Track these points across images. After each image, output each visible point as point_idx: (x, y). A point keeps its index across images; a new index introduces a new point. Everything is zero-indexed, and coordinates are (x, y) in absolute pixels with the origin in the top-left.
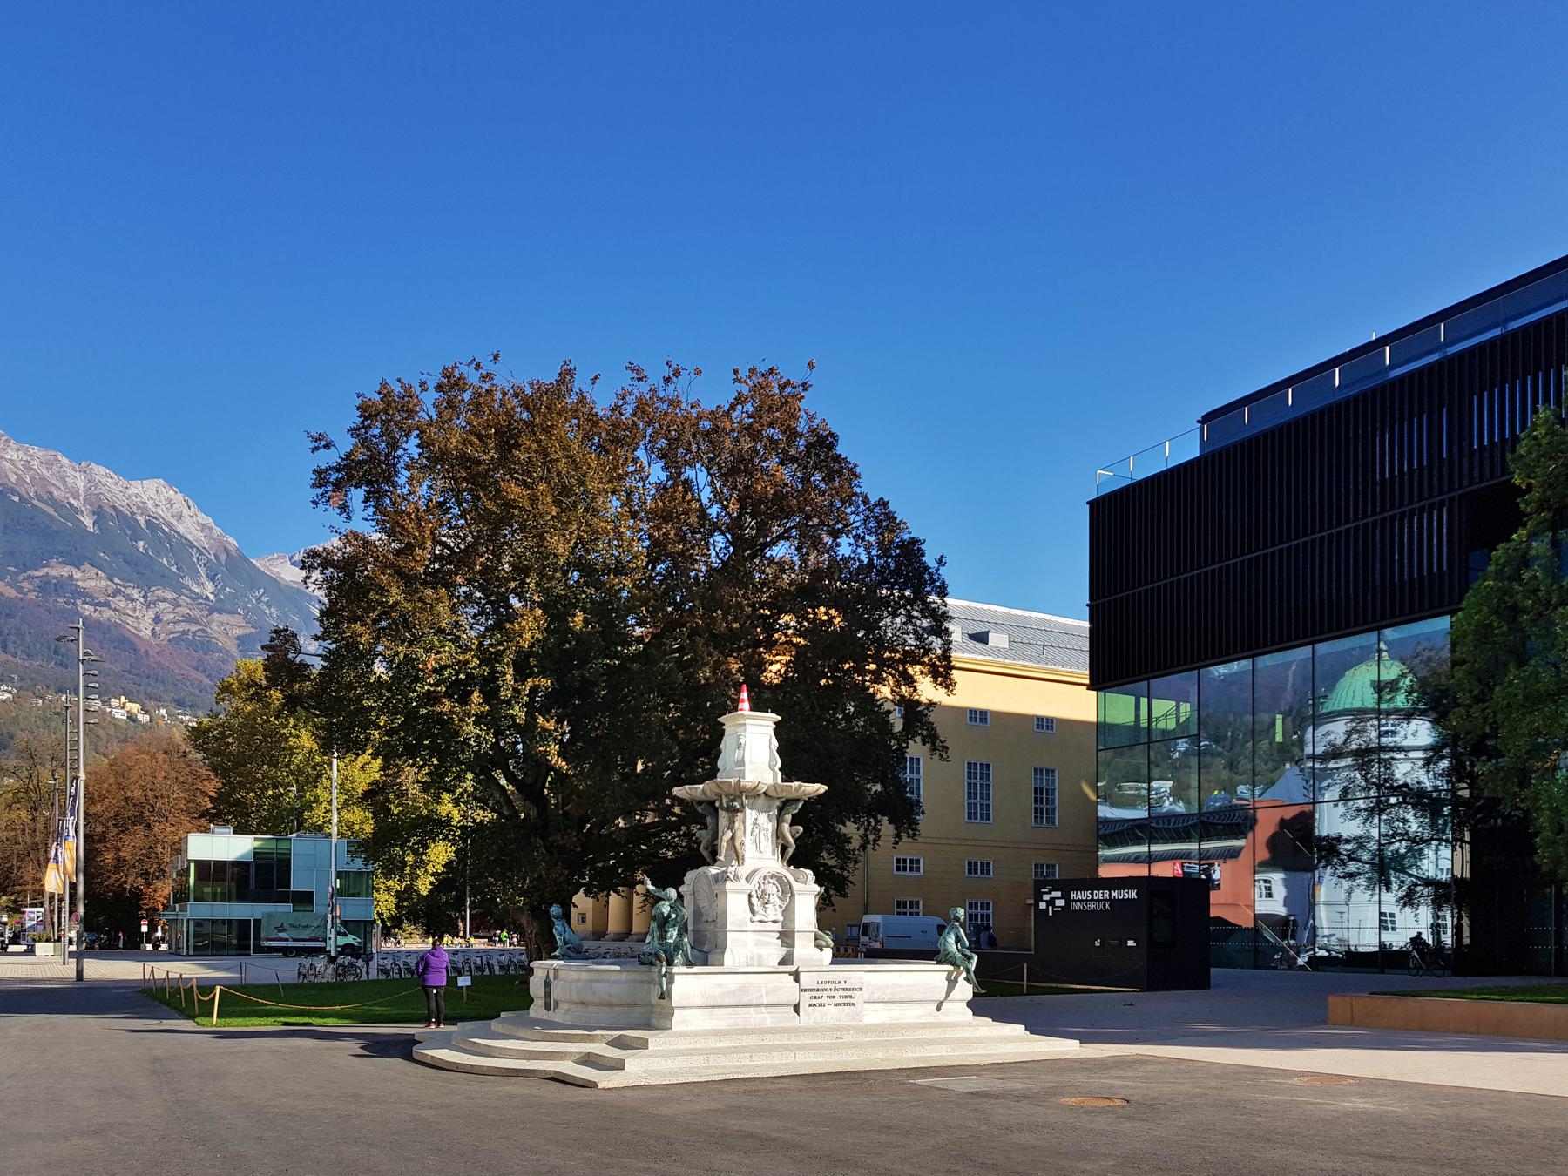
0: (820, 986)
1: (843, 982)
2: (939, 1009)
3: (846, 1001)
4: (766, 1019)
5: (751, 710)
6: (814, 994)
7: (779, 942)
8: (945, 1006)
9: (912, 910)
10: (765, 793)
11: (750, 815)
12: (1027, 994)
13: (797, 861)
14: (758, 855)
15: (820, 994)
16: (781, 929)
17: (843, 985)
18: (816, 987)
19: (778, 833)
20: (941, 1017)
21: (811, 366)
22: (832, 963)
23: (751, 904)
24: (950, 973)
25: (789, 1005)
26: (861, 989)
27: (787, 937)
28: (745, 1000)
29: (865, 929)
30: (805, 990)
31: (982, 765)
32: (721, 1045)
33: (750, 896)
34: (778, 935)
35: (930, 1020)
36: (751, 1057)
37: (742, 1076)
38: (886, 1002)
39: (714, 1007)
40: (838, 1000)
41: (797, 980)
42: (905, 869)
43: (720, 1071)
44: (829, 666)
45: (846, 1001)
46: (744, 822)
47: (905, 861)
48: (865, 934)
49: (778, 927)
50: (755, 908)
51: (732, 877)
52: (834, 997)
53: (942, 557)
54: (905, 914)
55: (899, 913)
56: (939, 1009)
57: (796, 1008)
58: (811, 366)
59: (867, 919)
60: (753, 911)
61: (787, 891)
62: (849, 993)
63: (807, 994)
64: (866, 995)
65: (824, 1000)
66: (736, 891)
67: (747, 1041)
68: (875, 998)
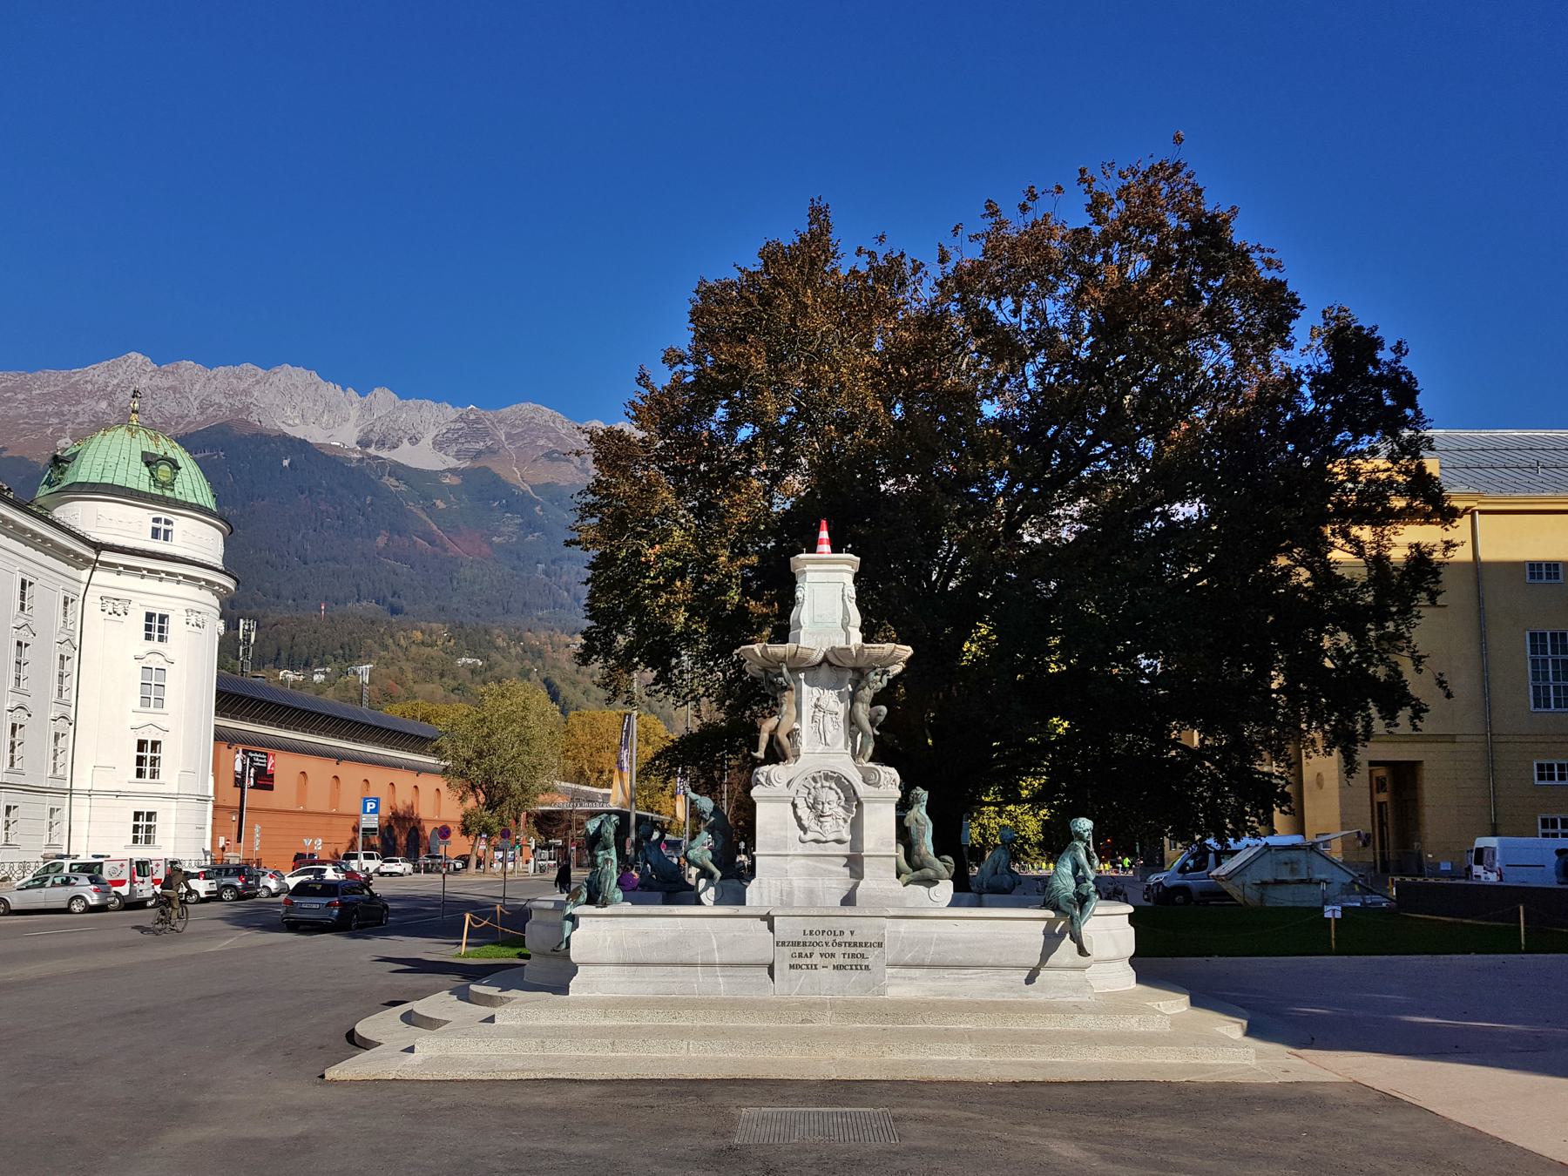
0: (809, 939)
1: (847, 933)
2: (1030, 980)
3: (855, 961)
4: (721, 985)
5: (833, 552)
6: (799, 950)
7: (847, 871)
8: (1044, 974)
9: (1546, 831)
10: (825, 660)
11: (809, 694)
12: (1526, 952)
13: (882, 755)
14: (820, 748)
15: (808, 950)
16: (849, 853)
17: (847, 938)
18: (801, 939)
19: (852, 721)
20: (1033, 994)
21: (1178, 140)
22: (954, 903)
23: (799, 819)
24: (1051, 923)
25: (762, 965)
26: (880, 945)
27: (855, 863)
28: (685, 956)
29: (1480, 855)
30: (783, 943)
31: (1553, 635)
32: (607, 1023)
33: (795, 806)
34: (845, 861)
35: (1011, 997)
36: (613, 1044)
37: (551, 1076)
38: (930, 966)
39: (731, 965)
40: (839, 960)
41: (771, 928)
42: (1551, 777)
43: (519, 1065)
44: (671, 444)
45: (855, 961)
46: (798, 705)
47: (1551, 767)
48: (1479, 861)
49: (845, 849)
50: (805, 823)
51: (762, 780)
52: (833, 955)
53: (1399, 343)
54: (1555, 835)
55: (1545, 835)
56: (1030, 980)
57: (771, 970)
58: (1178, 140)
59: (1482, 842)
60: (804, 829)
61: (852, 799)
62: (859, 950)
63: (787, 951)
64: (890, 954)
65: (816, 959)
66: (770, 799)
67: (649, 1020)
68: (908, 958)
